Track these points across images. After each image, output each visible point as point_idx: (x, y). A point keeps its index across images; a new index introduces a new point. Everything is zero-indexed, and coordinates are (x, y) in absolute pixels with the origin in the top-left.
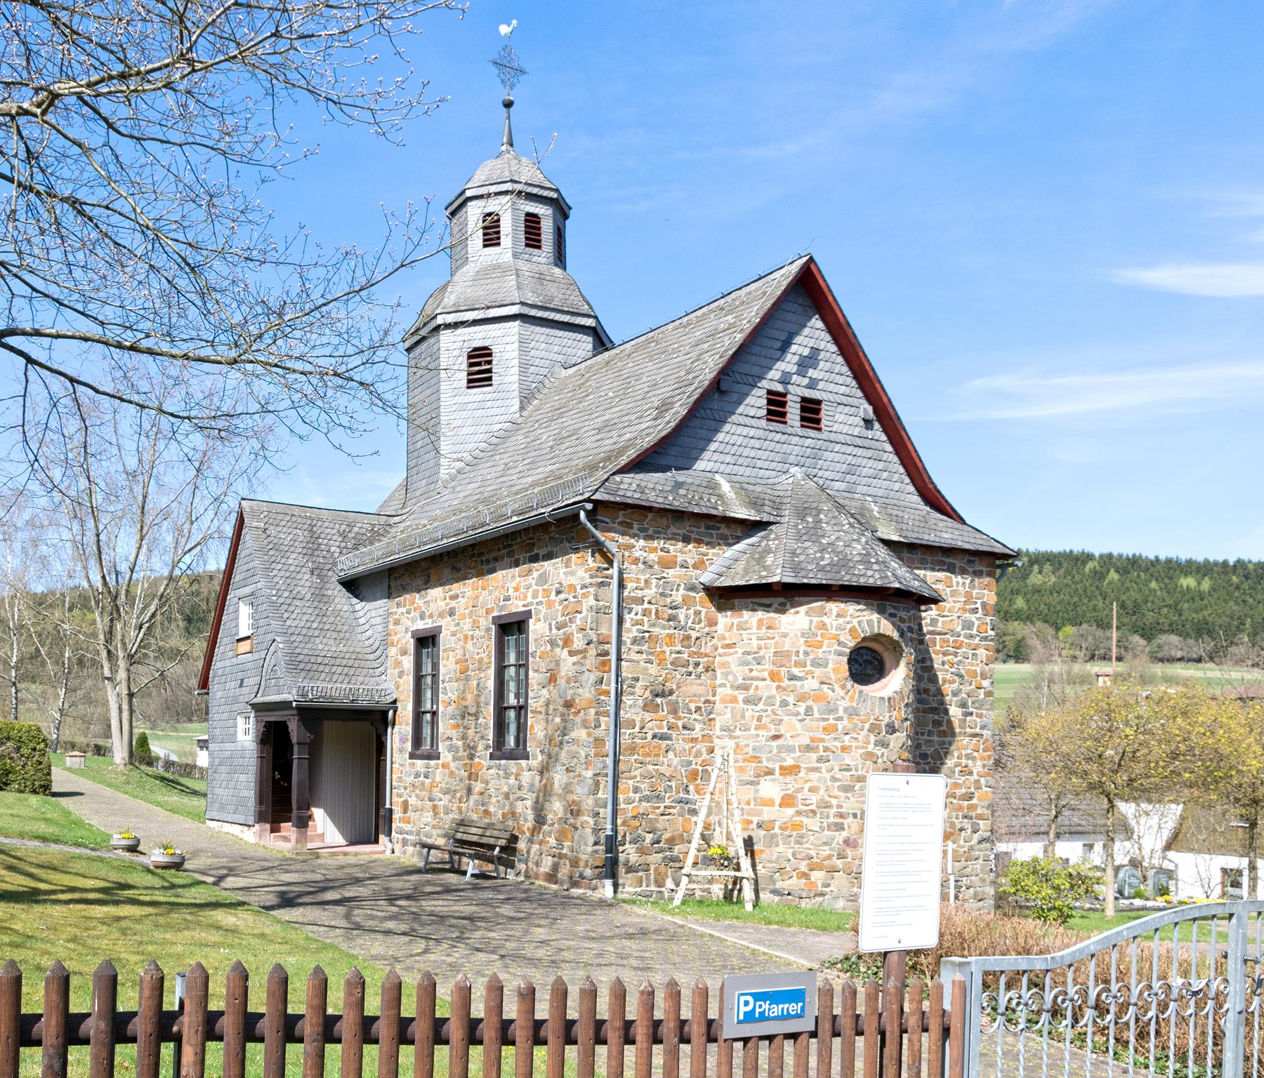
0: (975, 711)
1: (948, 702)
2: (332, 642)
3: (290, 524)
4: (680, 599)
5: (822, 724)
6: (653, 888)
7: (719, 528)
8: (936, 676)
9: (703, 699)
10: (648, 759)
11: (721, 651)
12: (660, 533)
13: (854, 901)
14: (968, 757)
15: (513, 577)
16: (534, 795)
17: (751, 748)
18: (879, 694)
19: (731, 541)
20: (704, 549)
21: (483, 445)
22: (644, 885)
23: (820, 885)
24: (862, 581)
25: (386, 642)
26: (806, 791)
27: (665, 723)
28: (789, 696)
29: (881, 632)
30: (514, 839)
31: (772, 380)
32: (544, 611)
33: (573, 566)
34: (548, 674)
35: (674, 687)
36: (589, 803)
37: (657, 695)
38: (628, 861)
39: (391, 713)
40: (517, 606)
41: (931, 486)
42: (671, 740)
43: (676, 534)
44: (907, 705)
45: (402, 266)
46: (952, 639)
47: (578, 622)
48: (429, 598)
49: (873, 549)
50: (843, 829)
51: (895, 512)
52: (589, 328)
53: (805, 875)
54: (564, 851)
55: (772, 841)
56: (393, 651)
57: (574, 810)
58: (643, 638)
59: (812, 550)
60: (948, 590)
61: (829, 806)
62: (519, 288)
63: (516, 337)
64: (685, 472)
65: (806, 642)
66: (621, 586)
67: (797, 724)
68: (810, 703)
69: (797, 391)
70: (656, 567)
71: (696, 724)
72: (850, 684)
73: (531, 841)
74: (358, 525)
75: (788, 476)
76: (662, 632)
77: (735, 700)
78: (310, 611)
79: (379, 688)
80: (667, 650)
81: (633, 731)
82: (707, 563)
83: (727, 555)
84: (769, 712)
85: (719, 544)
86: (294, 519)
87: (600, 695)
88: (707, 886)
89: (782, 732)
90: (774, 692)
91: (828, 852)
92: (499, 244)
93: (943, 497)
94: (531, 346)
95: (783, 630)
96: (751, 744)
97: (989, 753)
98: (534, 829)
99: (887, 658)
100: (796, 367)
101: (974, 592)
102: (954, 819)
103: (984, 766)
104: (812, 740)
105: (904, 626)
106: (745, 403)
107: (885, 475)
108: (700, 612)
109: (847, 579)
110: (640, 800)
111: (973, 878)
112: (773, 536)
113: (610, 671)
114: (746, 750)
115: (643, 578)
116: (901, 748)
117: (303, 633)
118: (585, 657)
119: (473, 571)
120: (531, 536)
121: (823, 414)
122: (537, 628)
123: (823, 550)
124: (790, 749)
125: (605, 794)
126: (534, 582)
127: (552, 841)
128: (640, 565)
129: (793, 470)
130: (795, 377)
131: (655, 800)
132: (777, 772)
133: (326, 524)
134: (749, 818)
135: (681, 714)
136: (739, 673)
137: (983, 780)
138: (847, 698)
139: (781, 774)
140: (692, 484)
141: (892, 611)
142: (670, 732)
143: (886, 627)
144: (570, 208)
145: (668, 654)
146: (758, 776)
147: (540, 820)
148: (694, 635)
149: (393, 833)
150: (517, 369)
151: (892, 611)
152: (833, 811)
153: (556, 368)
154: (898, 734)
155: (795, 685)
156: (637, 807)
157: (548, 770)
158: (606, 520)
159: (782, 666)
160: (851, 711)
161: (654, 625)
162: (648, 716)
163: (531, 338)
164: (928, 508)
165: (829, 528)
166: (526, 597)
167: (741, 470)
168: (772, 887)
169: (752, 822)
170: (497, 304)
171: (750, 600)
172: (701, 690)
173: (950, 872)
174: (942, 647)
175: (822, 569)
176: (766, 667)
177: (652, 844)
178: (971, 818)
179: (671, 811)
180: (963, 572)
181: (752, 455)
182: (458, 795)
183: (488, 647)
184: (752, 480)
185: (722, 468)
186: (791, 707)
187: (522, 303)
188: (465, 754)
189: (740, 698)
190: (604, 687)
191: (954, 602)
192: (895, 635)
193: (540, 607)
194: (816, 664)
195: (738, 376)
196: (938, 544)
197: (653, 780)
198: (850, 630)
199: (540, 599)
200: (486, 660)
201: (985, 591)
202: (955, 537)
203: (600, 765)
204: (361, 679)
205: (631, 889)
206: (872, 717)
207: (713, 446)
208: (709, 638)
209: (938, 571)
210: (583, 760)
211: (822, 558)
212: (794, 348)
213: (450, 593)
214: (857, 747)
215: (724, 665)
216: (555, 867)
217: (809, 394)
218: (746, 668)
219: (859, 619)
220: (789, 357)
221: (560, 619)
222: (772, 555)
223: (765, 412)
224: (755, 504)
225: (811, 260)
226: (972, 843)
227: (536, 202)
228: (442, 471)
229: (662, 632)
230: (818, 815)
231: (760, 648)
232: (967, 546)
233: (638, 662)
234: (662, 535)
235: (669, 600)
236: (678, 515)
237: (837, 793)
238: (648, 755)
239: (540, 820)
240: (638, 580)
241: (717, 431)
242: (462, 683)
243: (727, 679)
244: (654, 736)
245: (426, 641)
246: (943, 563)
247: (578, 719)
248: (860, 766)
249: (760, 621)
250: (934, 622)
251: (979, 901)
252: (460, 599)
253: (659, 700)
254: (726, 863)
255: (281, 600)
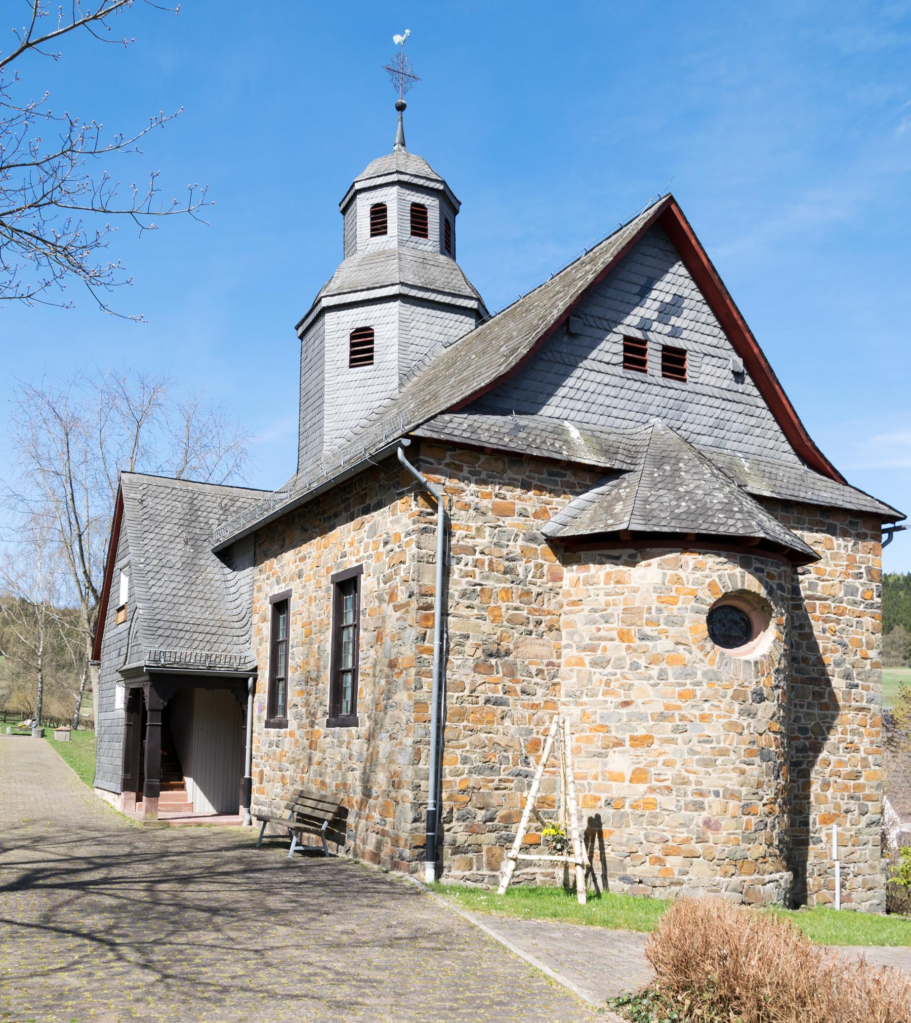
0: (860, 682)
1: (830, 673)
2: (197, 609)
3: (169, 496)
4: (518, 551)
5: (677, 689)
6: (485, 871)
7: (564, 476)
8: (816, 644)
9: (545, 661)
10: (479, 726)
11: (566, 608)
12: (495, 477)
13: (716, 891)
14: (853, 732)
15: (349, 531)
16: (362, 765)
17: (598, 716)
18: (747, 657)
19: (578, 490)
20: (546, 497)
21: (364, 422)
22: (475, 868)
23: (676, 872)
24: (722, 530)
25: (251, 611)
26: (660, 764)
27: (500, 687)
28: (639, 658)
29: (746, 588)
30: (342, 812)
31: (629, 325)
32: (373, 564)
33: (399, 513)
34: (376, 633)
35: (511, 647)
36: (408, 774)
37: (491, 655)
38: (455, 841)
39: (250, 681)
40: (351, 563)
41: (809, 444)
42: (508, 705)
43: (514, 479)
44: (777, 671)
45: (29, 45)
46: (833, 605)
47: (402, 574)
48: (284, 562)
49: (738, 499)
50: (703, 809)
51: (768, 469)
52: (471, 309)
53: (659, 861)
54: (387, 828)
55: (622, 821)
56: (256, 618)
57: (396, 784)
58: (474, 591)
59: (667, 498)
60: (828, 552)
61: (686, 782)
62: (400, 270)
63: (397, 317)
64: (528, 416)
65: (659, 597)
66: (448, 532)
67: (650, 689)
68: (664, 665)
69: (658, 338)
70: (490, 514)
71: (538, 688)
72: (709, 644)
73: (358, 815)
74: (241, 500)
75: (647, 426)
76: (497, 585)
77: (581, 662)
78: (179, 579)
79: (243, 655)
80: (504, 605)
81: (461, 694)
82: (551, 512)
83: (573, 504)
84: (618, 676)
85: (565, 493)
86: (174, 492)
87: (421, 652)
88: (550, 870)
89: (633, 699)
90: (624, 653)
91: (685, 835)
92: (385, 233)
93: (822, 456)
94: (412, 325)
95: (633, 584)
96: (599, 712)
97: (876, 729)
98: (362, 801)
99: (755, 618)
100: (657, 314)
101: (858, 556)
102: (839, 800)
103: (872, 743)
104: (667, 707)
105: (774, 583)
106: (599, 347)
107: (758, 431)
108: (542, 566)
109: (704, 527)
110: (470, 772)
111: (862, 864)
112: (624, 484)
113: (432, 627)
114: (593, 718)
115: (473, 525)
116: (772, 718)
117: (167, 600)
118: (407, 611)
119: (317, 530)
120: (364, 486)
121: (687, 364)
122: (367, 583)
123: (679, 498)
124: (642, 718)
125: (427, 765)
126: (366, 534)
127: (376, 816)
128: (471, 511)
129: (653, 420)
130: (655, 324)
131: (488, 772)
132: (628, 743)
133: (208, 498)
134: (597, 794)
135: (519, 677)
136: (586, 632)
137: (871, 758)
138: (707, 660)
139: (631, 746)
140: (535, 428)
141: (759, 565)
142: (506, 696)
143: (752, 583)
144: (460, 203)
145: (504, 610)
146: (607, 747)
147: (367, 793)
148: (535, 590)
149: (252, 804)
150: (397, 347)
151: (759, 565)
152: (691, 788)
153: (437, 347)
154: (767, 702)
155: (647, 646)
156: (465, 779)
157: (373, 736)
158: (431, 460)
159: (632, 624)
160: (711, 675)
161: (487, 578)
162: (479, 678)
163: (412, 318)
164: (806, 468)
165: (689, 476)
166: (359, 551)
167: (595, 418)
168: (621, 873)
169: (599, 799)
170: (378, 285)
171: (597, 552)
172: (543, 651)
173: (835, 857)
174: (822, 613)
175: (677, 517)
176: (615, 625)
177: (485, 822)
178: (858, 799)
179: (506, 785)
180: (845, 534)
181: (607, 403)
182: (301, 764)
183: (327, 607)
184: (605, 429)
185: (573, 415)
186: (643, 670)
187: (402, 284)
188: (307, 721)
189: (587, 660)
190: (426, 644)
191: (836, 566)
192: (763, 592)
193: (370, 561)
194: (671, 622)
195: (590, 319)
196: (815, 503)
197: (486, 749)
198: (709, 585)
199: (370, 552)
200: (326, 622)
201: (870, 555)
202: (835, 497)
203: (421, 732)
204: (223, 646)
205: (459, 873)
206: (736, 683)
207: (562, 392)
208: (552, 594)
209: (817, 532)
210: (404, 726)
211: (678, 506)
212: (654, 294)
213: (300, 555)
214: (719, 717)
215: (569, 624)
216: (379, 845)
217: (671, 342)
218: (594, 627)
219: (720, 572)
220: (649, 302)
221: (387, 571)
222: (621, 503)
223: (621, 359)
224: (606, 451)
225: (671, 200)
226: (860, 826)
227: (422, 193)
228: (325, 448)
229: (497, 585)
230: (674, 792)
231: (608, 605)
232: (848, 506)
233: (468, 618)
234: (497, 480)
235: (505, 551)
236: (515, 458)
237: (695, 767)
238: (480, 721)
239: (367, 793)
240: (468, 528)
241: (567, 375)
242: (306, 647)
243: (573, 639)
244: (487, 701)
245: (281, 606)
246: (823, 524)
247: (400, 681)
248: (722, 738)
249: (608, 575)
250: (812, 586)
251: (869, 890)
252: (307, 560)
253: (493, 661)
254: (559, 846)
255: (149, 568)
